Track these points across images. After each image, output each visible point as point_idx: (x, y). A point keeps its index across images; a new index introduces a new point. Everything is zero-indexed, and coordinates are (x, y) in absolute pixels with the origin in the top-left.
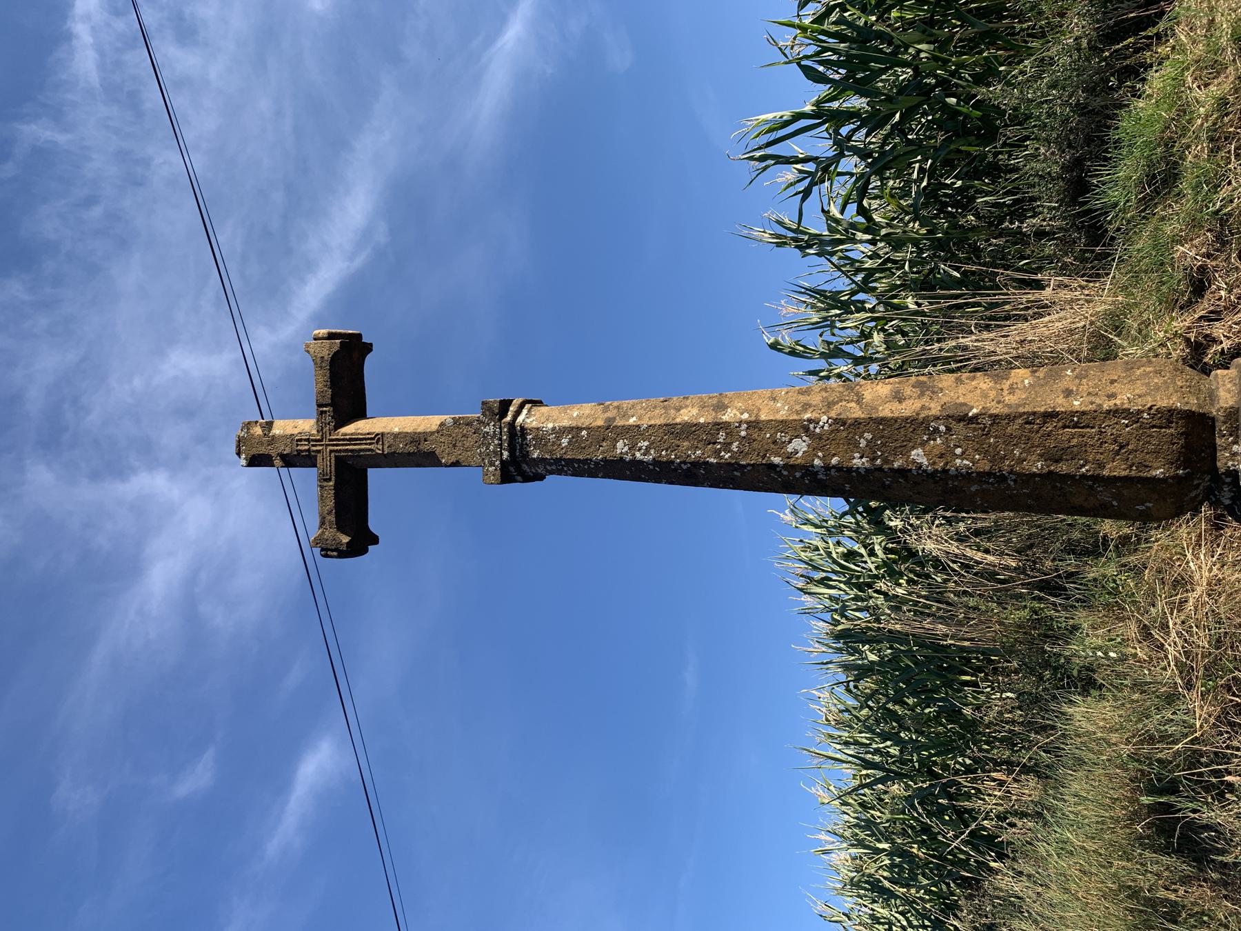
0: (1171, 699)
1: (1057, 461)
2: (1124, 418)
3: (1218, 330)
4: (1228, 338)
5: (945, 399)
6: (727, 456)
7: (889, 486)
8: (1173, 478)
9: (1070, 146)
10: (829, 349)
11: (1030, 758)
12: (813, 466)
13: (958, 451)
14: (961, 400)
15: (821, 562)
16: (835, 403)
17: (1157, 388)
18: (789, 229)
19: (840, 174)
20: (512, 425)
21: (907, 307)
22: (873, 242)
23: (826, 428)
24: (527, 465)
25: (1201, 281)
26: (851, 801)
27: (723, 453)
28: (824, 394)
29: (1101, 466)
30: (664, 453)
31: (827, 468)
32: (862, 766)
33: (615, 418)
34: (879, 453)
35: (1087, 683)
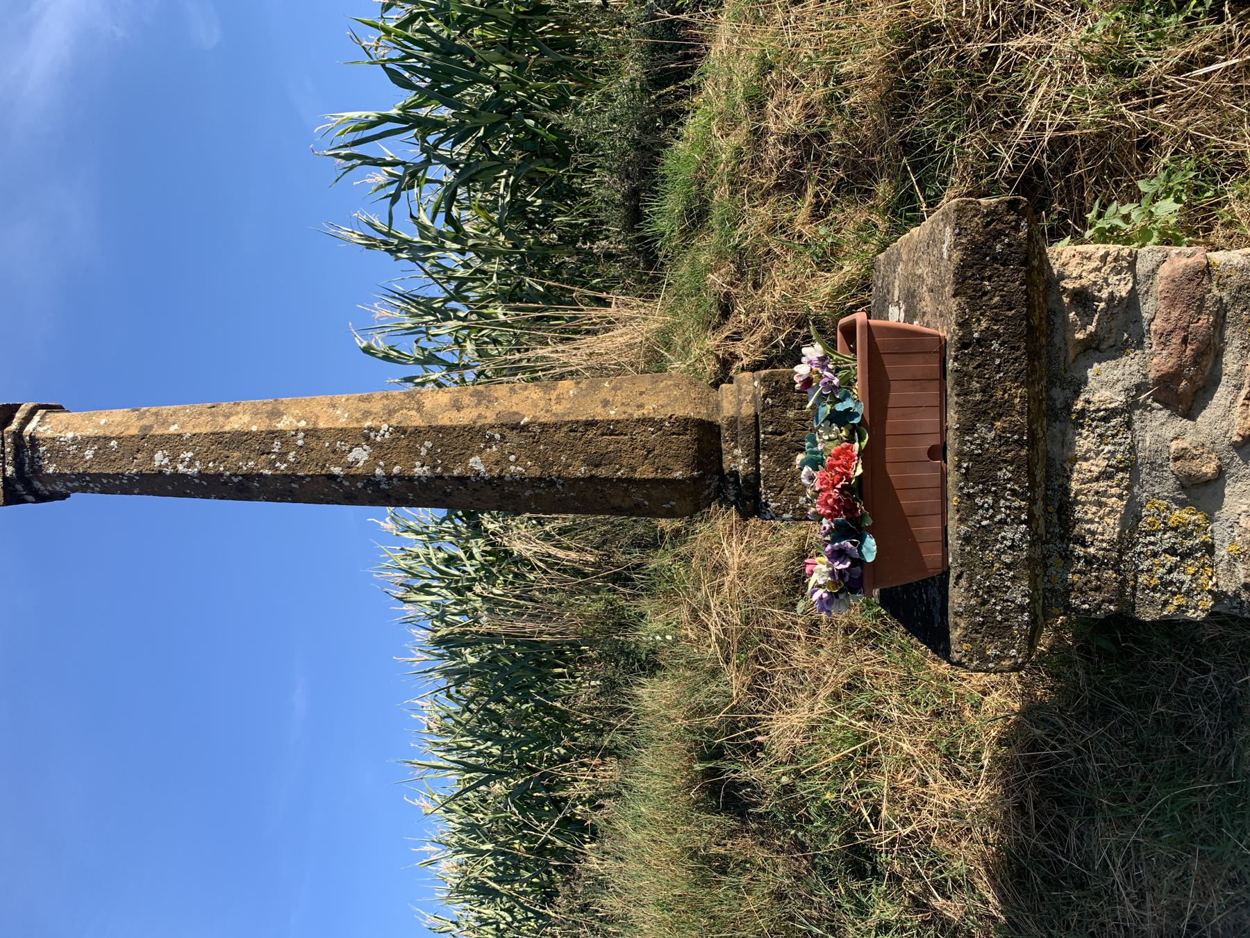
0: (715, 673)
1: (597, 466)
2: (650, 426)
3: (739, 348)
4: (747, 355)
5: (500, 408)
6: (283, 467)
7: (450, 494)
8: (689, 479)
9: (628, 176)
10: (424, 356)
11: (611, 741)
12: (374, 476)
13: (512, 458)
14: (514, 409)
15: (421, 569)
16: (395, 411)
17: (676, 400)
18: (380, 231)
19: (428, 181)
20: (18, 435)
21: (497, 317)
22: (462, 252)
23: (387, 436)
24: (41, 482)
25: (727, 306)
26: (455, 807)
27: (278, 464)
28: (386, 402)
29: (634, 469)
30: (211, 465)
31: (389, 477)
32: (464, 770)
33: (151, 427)
34: (440, 461)
35: (650, 666)
